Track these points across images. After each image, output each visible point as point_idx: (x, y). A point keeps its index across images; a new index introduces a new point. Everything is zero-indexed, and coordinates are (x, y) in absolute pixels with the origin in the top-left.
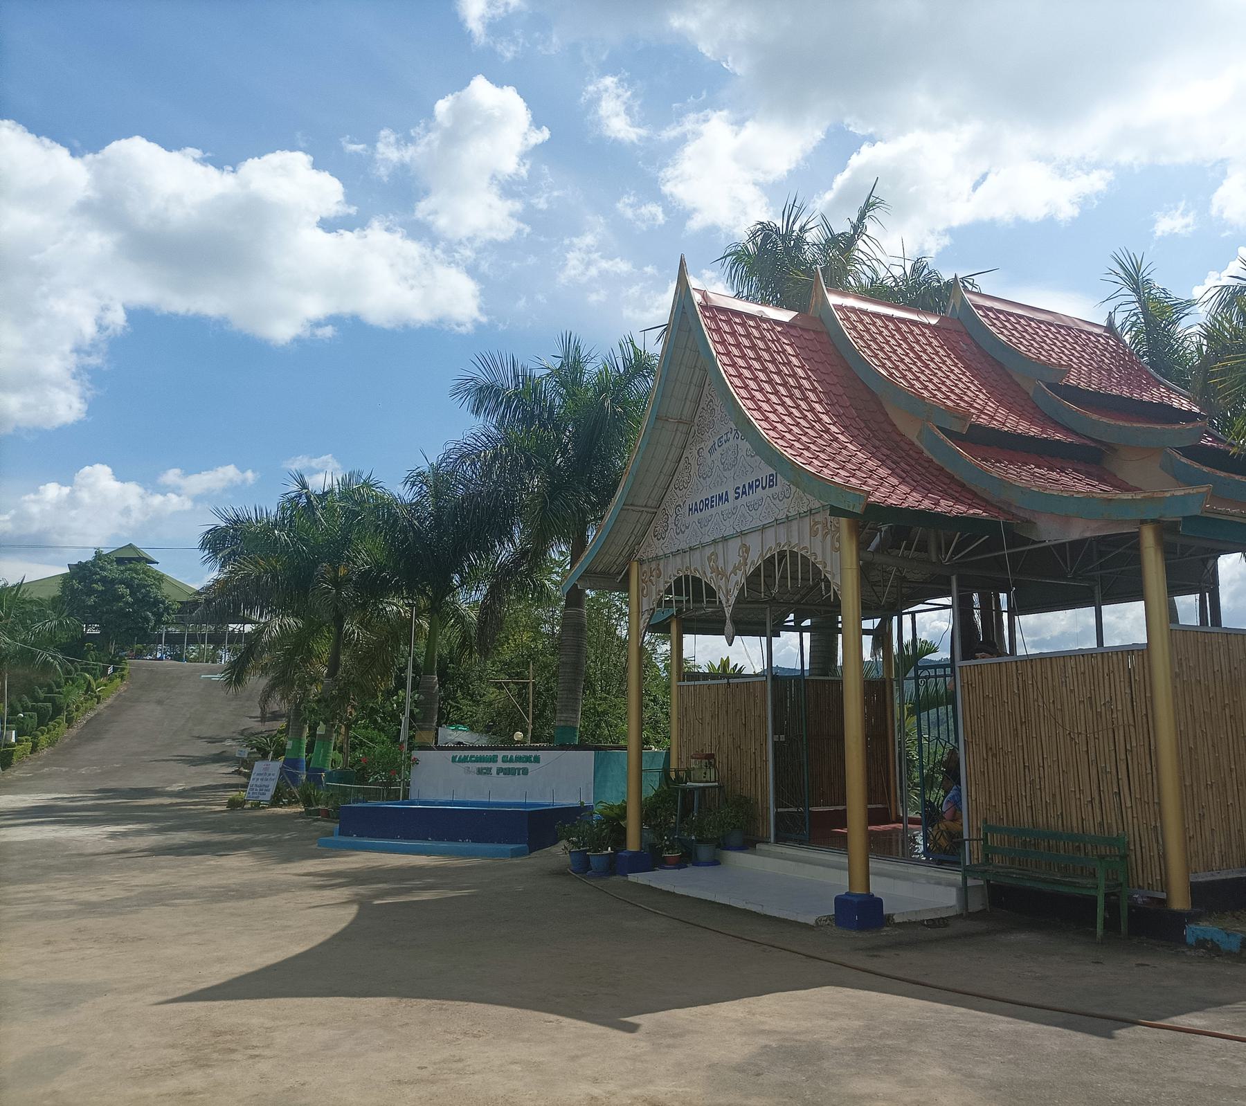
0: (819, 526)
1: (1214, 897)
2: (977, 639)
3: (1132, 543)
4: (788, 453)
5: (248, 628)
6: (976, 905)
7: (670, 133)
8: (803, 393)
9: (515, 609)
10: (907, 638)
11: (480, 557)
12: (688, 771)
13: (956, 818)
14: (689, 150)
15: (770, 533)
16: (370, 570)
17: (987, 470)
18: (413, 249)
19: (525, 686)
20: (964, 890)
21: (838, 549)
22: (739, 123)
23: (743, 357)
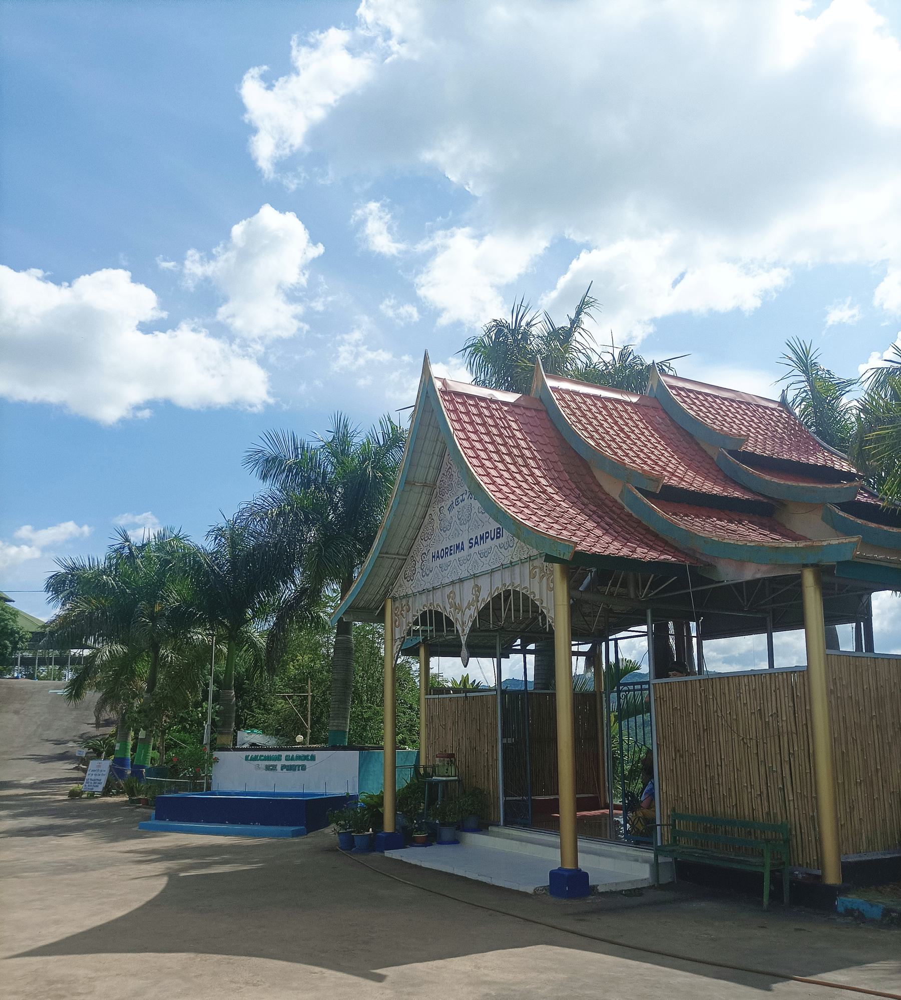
0: (537, 570)
1: (858, 874)
2: (669, 660)
3: (797, 581)
4: (511, 511)
5: (86, 652)
6: (666, 877)
7: (422, 247)
8: (524, 461)
9: (297, 635)
10: (612, 659)
11: (268, 596)
12: (434, 767)
13: (651, 806)
14: (440, 259)
15: (497, 575)
16: (180, 607)
17: (676, 523)
18: (214, 345)
19: (306, 698)
20: (656, 867)
21: (552, 589)
22: (479, 237)
23: (476, 432)
